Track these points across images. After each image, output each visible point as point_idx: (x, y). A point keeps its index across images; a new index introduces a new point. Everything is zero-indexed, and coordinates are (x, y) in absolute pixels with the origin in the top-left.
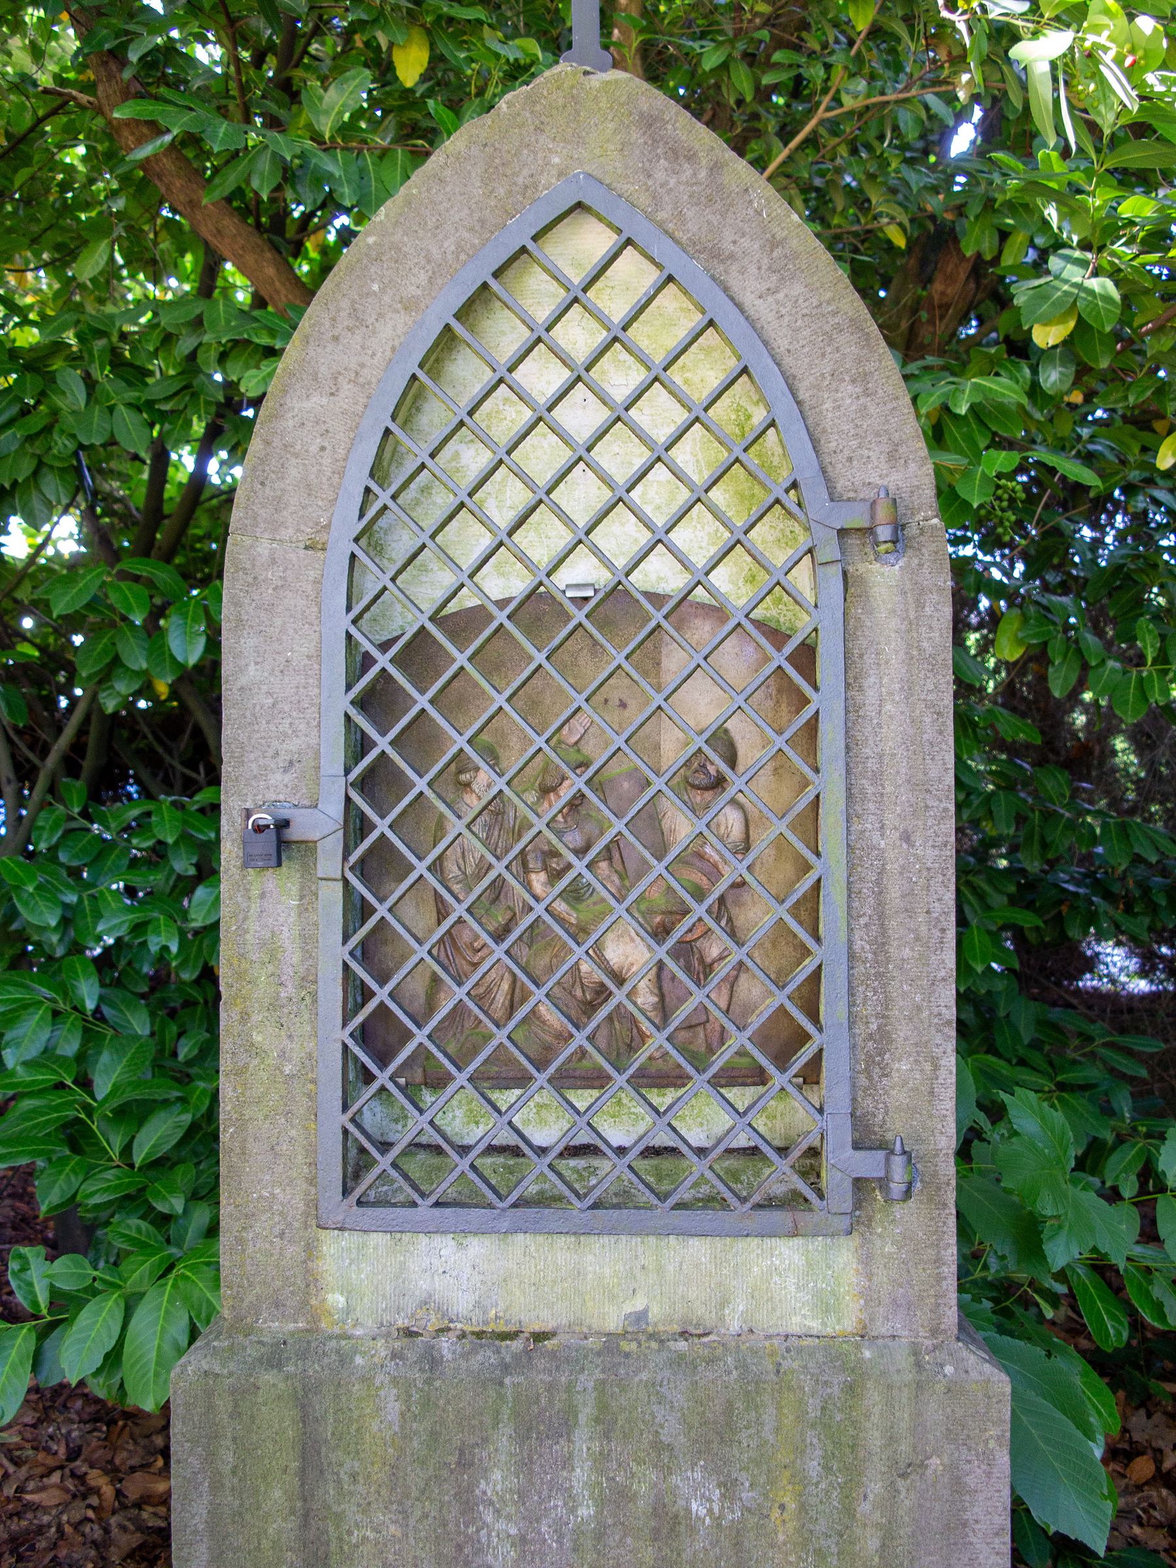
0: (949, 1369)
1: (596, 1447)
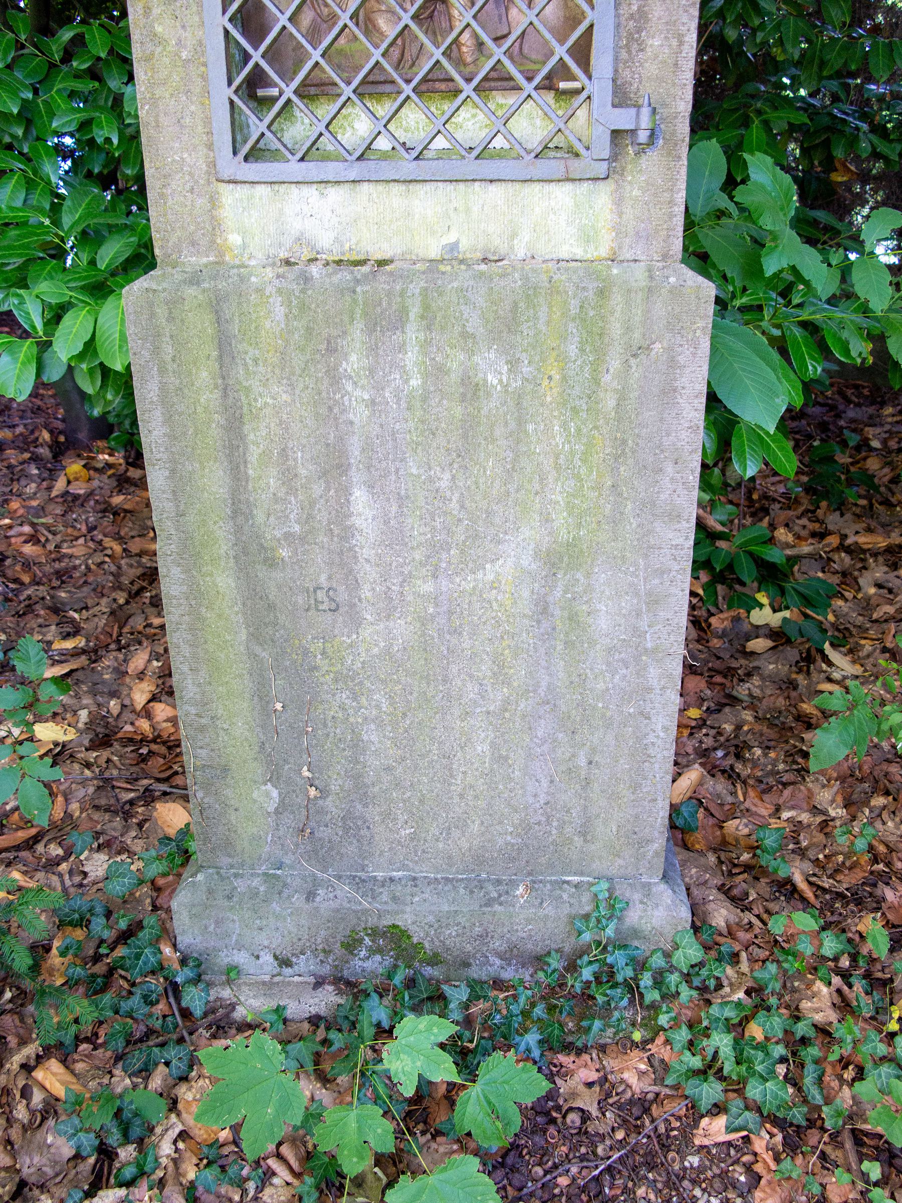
0: (672, 280)
1: (422, 336)
